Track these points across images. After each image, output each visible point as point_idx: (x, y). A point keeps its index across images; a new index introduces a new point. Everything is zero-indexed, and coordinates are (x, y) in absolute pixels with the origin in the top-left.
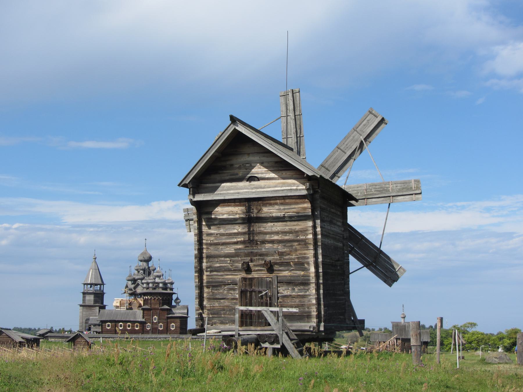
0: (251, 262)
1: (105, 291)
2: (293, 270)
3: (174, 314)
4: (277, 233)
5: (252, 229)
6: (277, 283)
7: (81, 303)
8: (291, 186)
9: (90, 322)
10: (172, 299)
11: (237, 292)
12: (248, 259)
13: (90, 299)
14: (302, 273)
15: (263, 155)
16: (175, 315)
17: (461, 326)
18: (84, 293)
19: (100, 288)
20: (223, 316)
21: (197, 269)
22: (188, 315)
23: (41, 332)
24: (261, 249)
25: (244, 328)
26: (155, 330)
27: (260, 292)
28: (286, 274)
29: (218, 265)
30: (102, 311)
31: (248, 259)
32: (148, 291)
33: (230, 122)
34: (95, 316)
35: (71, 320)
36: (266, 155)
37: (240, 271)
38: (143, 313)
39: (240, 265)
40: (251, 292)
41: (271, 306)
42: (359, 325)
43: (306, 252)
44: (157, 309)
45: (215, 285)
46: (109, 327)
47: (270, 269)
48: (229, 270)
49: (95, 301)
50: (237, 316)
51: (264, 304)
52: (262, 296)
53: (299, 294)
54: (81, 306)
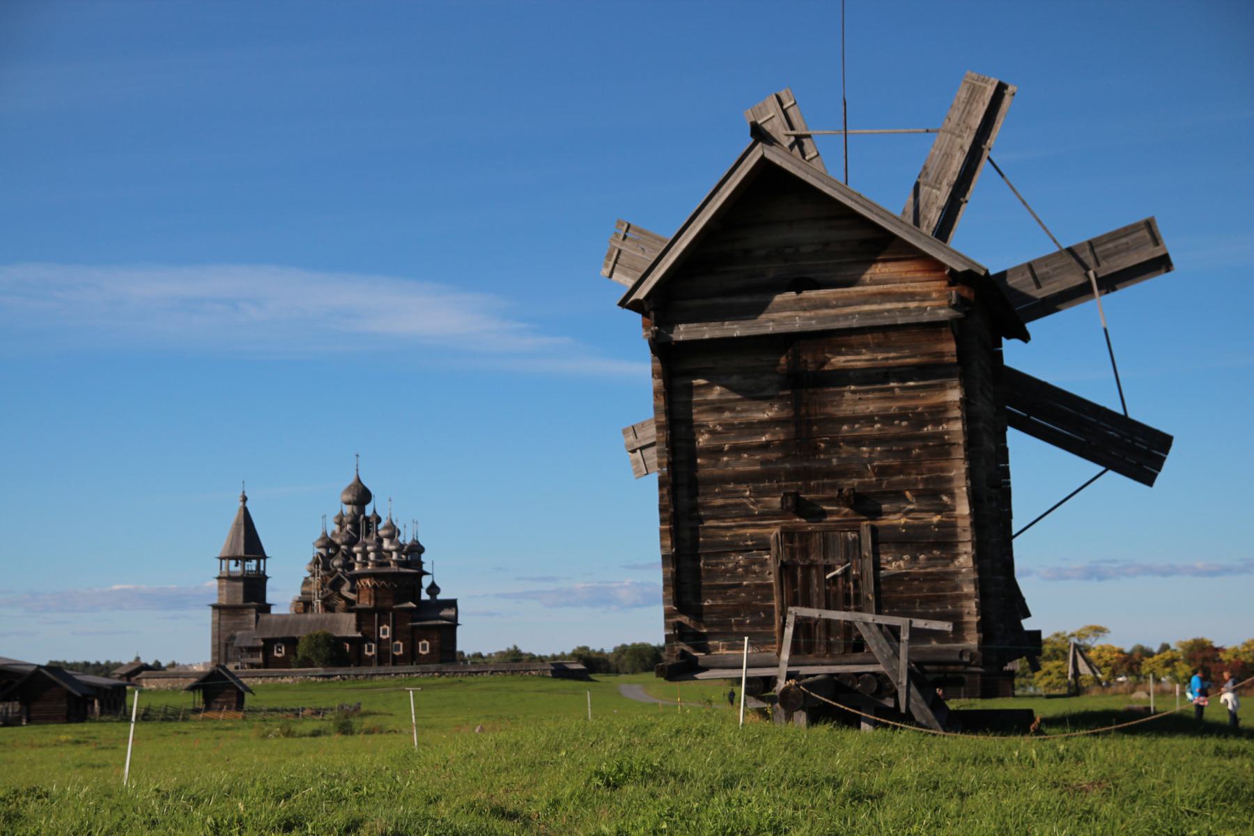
1: (267, 574)
4: (869, 419)
5: (803, 411)
6: (876, 543)
8: (906, 301)
10: (421, 586)
17: (1073, 635)
19: (258, 566)
20: (735, 629)
21: (666, 515)
23: (122, 671)
24: (829, 461)
26: (383, 657)
27: (830, 568)
28: (895, 522)
30: (264, 617)
33: (751, 140)
34: (249, 632)
39: (776, 502)
43: (944, 464)
46: (280, 650)
48: (750, 515)
49: (247, 597)
52: (835, 577)
53: (929, 570)
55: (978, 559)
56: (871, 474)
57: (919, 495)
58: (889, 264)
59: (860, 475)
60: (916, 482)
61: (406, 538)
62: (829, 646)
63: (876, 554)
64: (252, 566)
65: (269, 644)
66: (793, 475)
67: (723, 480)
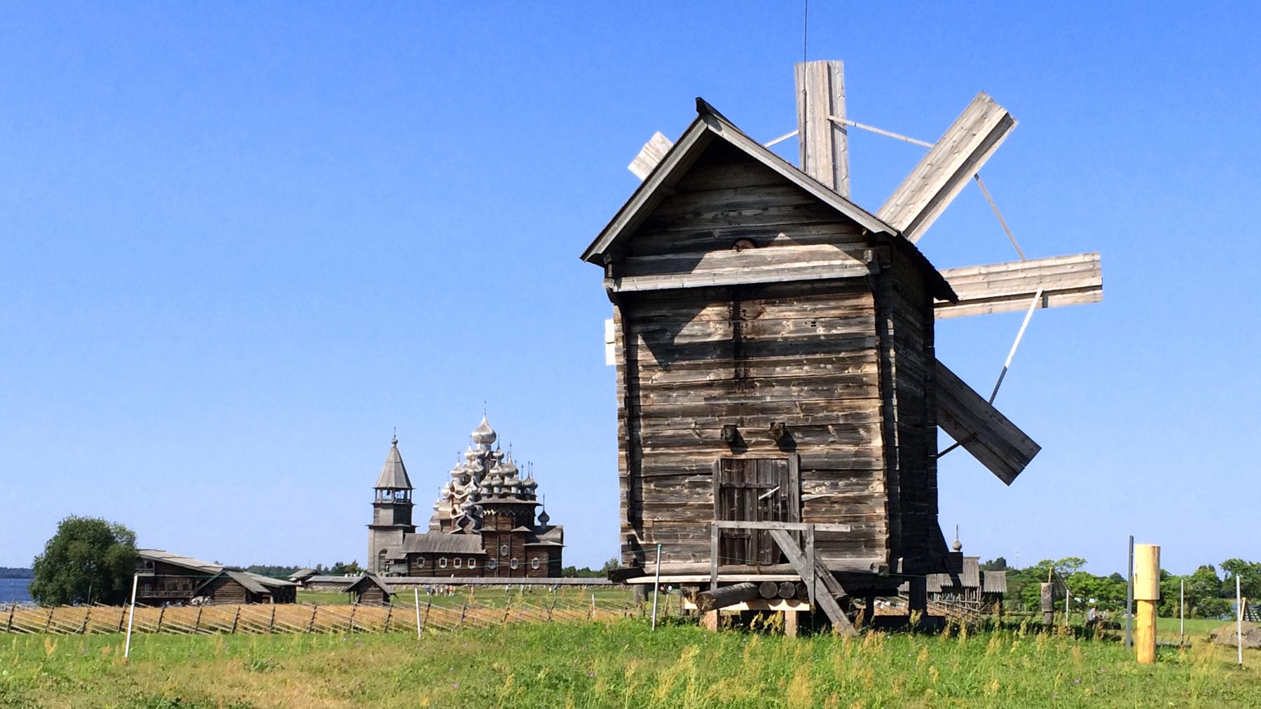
0: (742, 426)
2: (833, 442)
3: (538, 541)
6: (800, 471)
7: (371, 523)
9: (387, 556)
11: (712, 491)
12: (732, 419)
13: (387, 516)
14: (852, 449)
15: (768, 190)
16: (542, 543)
18: (376, 505)
19: (405, 495)
20: (680, 542)
22: (561, 540)
25: (727, 567)
26: (503, 571)
27: (762, 490)
29: (670, 432)
30: (407, 535)
31: (732, 419)
32: (491, 500)
34: (397, 545)
35: (358, 549)
36: (779, 190)
37: (716, 444)
38: (483, 540)
39: (717, 433)
40: (742, 491)
41: (785, 520)
42: (953, 563)
44: (509, 532)
45: (667, 477)
46: (423, 562)
47: (785, 441)
50: (715, 539)
51: (770, 515)
52: (766, 499)
54: (371, 527)
55: (887, 485)
56: (798, 410)
57: (840, 429)
58: (819, 227)
59: (789, 411)
60: (838, 418)
61: (522, 478)
62: (759, 557)
63: (801, 480)
64: (400, 495)
65: (411, 557)
66: (733, 410)
67: (673, 414)
